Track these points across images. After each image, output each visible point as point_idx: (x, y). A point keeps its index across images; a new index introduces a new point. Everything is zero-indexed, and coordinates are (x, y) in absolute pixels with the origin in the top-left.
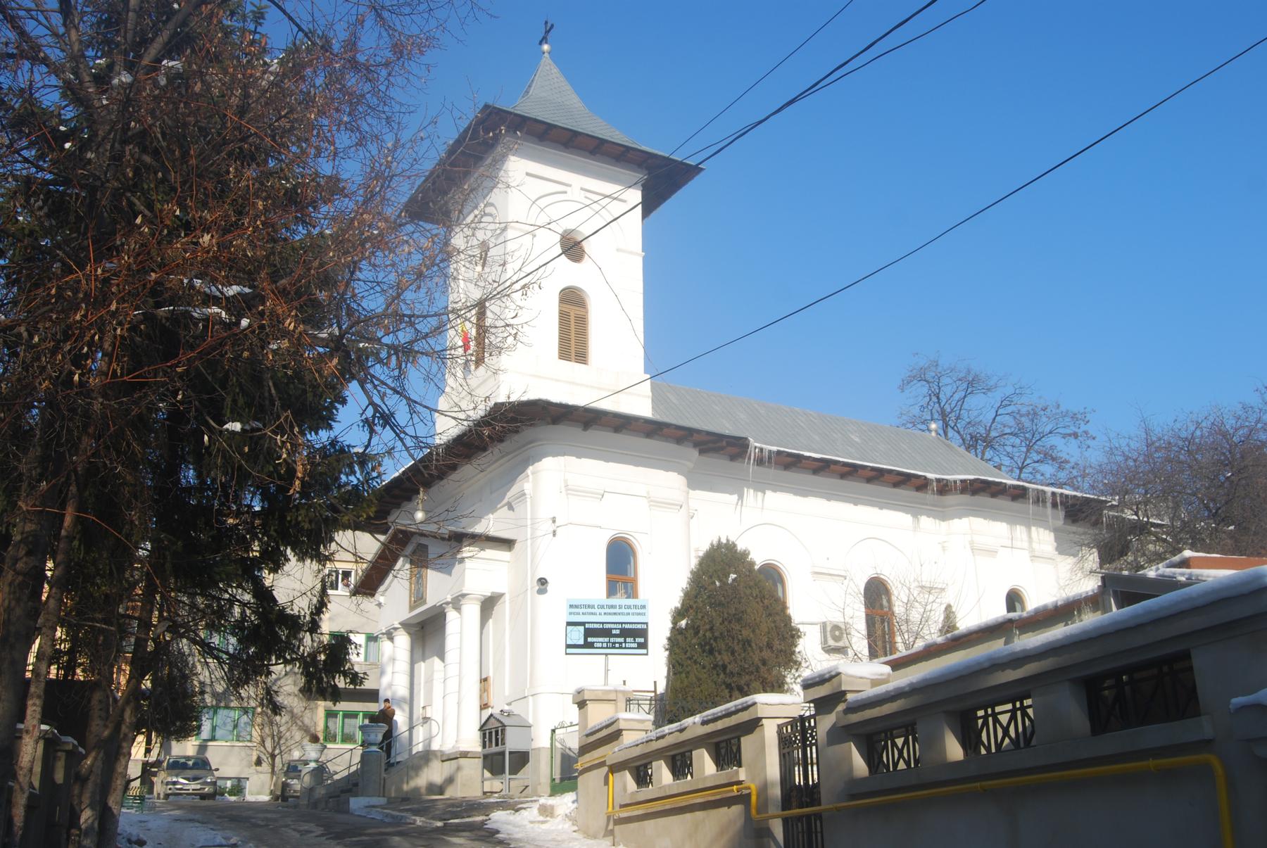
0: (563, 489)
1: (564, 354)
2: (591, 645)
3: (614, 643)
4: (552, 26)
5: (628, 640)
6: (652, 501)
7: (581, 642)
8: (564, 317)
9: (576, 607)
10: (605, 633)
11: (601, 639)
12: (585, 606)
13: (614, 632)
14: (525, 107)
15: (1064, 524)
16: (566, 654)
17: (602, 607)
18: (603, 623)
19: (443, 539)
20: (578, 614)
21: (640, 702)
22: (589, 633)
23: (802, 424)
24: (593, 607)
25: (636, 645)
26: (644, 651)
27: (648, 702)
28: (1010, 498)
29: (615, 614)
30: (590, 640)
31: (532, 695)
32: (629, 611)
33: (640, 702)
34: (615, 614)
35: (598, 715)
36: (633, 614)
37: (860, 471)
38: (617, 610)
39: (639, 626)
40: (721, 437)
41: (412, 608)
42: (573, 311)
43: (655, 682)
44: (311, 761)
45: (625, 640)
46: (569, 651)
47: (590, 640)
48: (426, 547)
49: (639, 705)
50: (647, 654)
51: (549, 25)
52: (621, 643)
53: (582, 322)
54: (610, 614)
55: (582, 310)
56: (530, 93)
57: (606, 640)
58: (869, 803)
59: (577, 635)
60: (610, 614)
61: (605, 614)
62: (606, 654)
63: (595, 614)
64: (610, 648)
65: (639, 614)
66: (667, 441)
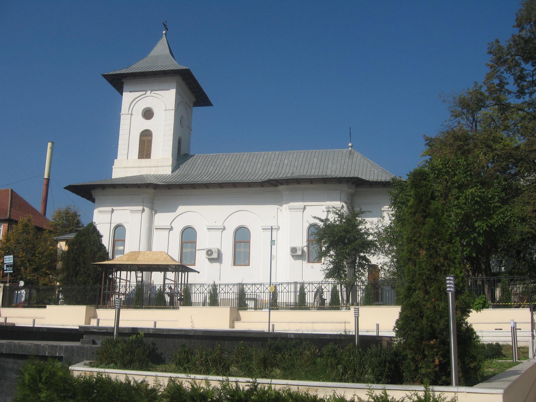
30: (7, 268)
55: (150, 137)
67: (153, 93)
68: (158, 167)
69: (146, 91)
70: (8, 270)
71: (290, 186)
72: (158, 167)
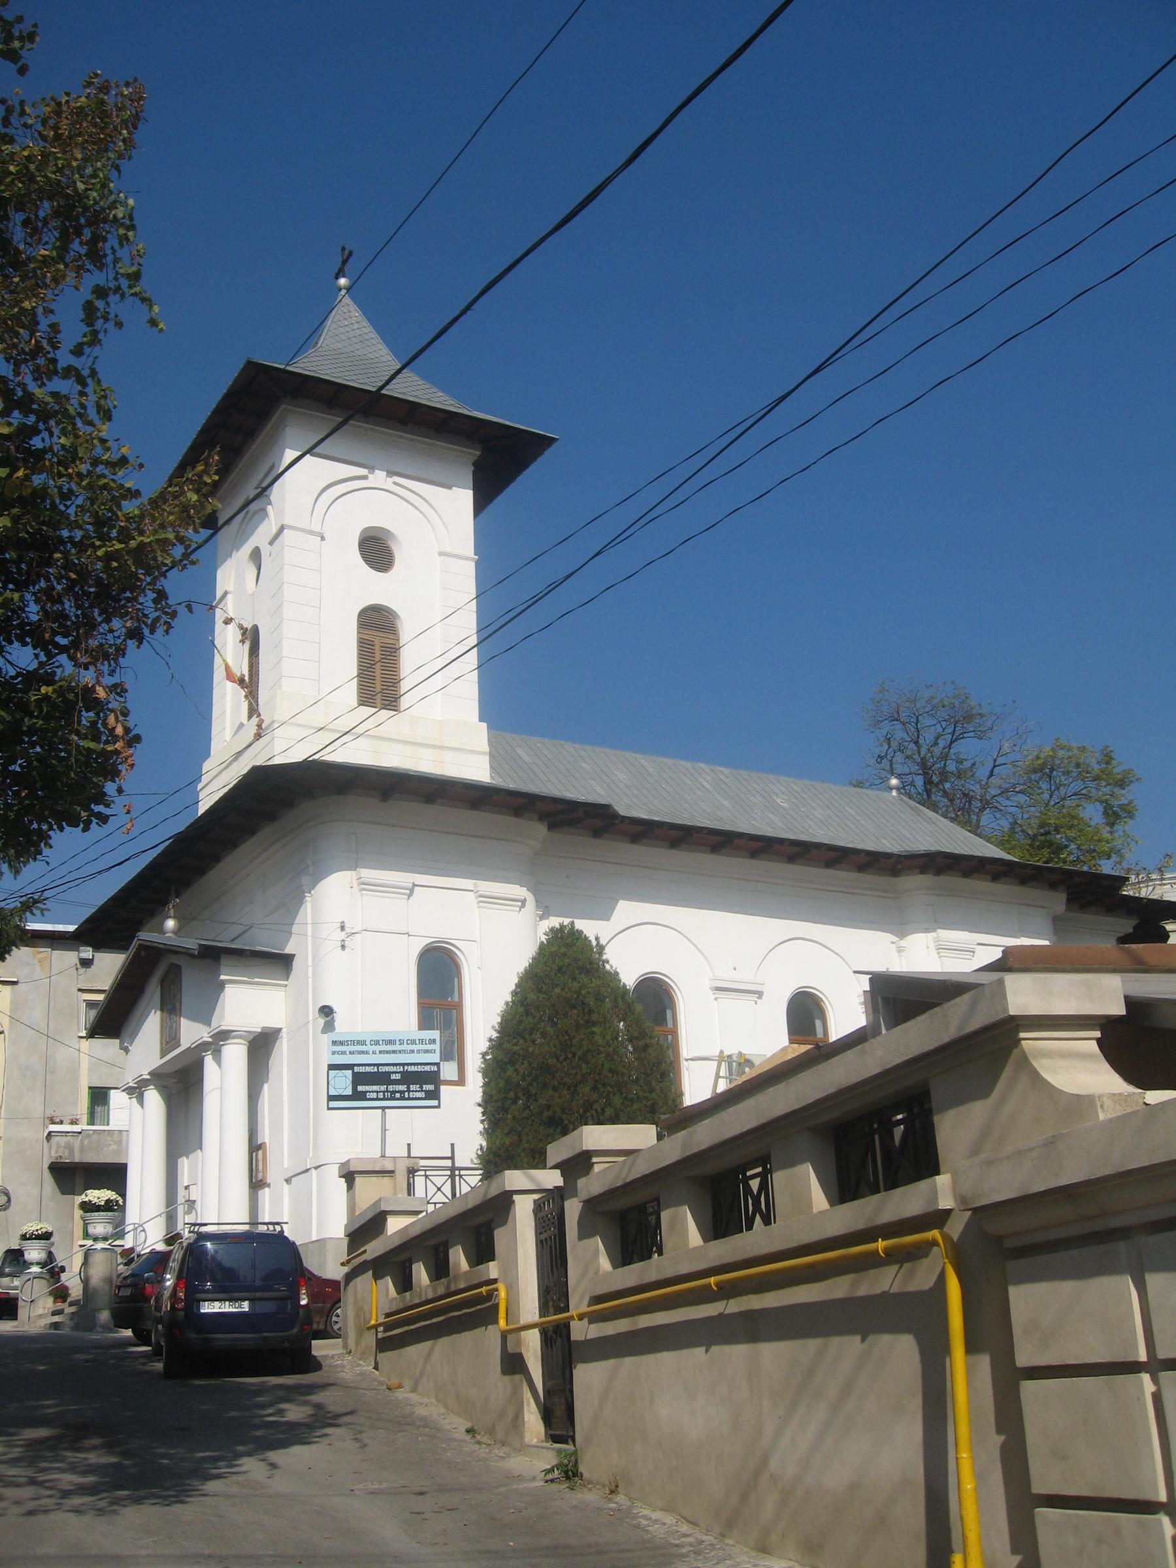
0: (355, 884)
1: (367, 697)
2: (362, 1096)
3: (394, 1092)
4: (351, 253)
5: (413, 1087)
6: (480, 896)
7: (349, 1092)
8: (365, 647)
9: (342, 1043)
10: (379, 1077)
11: (375, 1088)
12: (353, 1042)
13: (393, 1077)
14: (309, 364)
15: (1066, 910)
16: (329, 1109)
17: (377, 1043)
18: (378, 1065)
19: (192, 956)
20: (344, 1053)
21: (462, 1172)
22: (358, 1079)
23: (708, 786)
24: (363, 1043)
25: (422, 1095)
26: (434, 1103)
27: (448, 1173)
28: (989, 877)
29: (394, 1052)
30: (360, 1088)
31: (316, 1168)
32: (411, 1047)
33: (428, 1173)
34: (394, 1052)
35: (370, 1192)
36: (419, 1051)
37: (735, 840)
38: (397, 1047)
39: (427, 1068)
40: (573, 805)
41: (163, 1053)
42: (378, 639)
43: (452, 1145)
44: (32, 1264)
45: (408, 1088)
46: (333, 1104)
47: (360, 1088)
48: (179, 967)
49: (426, 1176)
50: (438, 1107)
51: (347, 251)
52: (402, 1092)
53: (392, 652)
54: (388, 1052)
56: (319, 345)
57: (383, 1088)
58: (614, 1307)
59: (343, 1083)
60: (388, 1052)
61: (381, 1052)
62: (383, 1108)
63: (367, 1053)
64: (397, 1099)
65: (427, 1051)
66: (500, 813)
67: (395, 483)
68: (442, 748)
69: (371, 469)
70: (369, 1095)
71: (946, 880)
72: (442, 748)
